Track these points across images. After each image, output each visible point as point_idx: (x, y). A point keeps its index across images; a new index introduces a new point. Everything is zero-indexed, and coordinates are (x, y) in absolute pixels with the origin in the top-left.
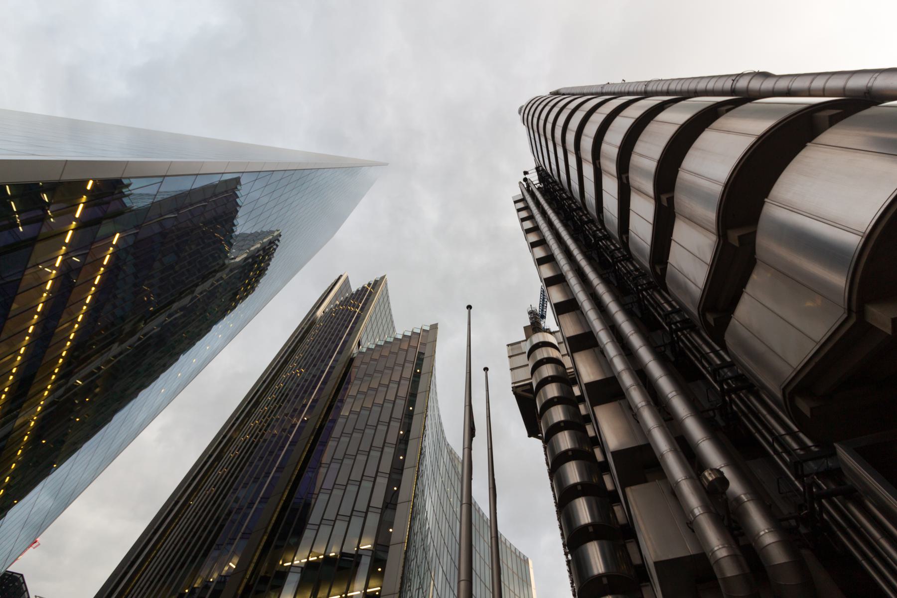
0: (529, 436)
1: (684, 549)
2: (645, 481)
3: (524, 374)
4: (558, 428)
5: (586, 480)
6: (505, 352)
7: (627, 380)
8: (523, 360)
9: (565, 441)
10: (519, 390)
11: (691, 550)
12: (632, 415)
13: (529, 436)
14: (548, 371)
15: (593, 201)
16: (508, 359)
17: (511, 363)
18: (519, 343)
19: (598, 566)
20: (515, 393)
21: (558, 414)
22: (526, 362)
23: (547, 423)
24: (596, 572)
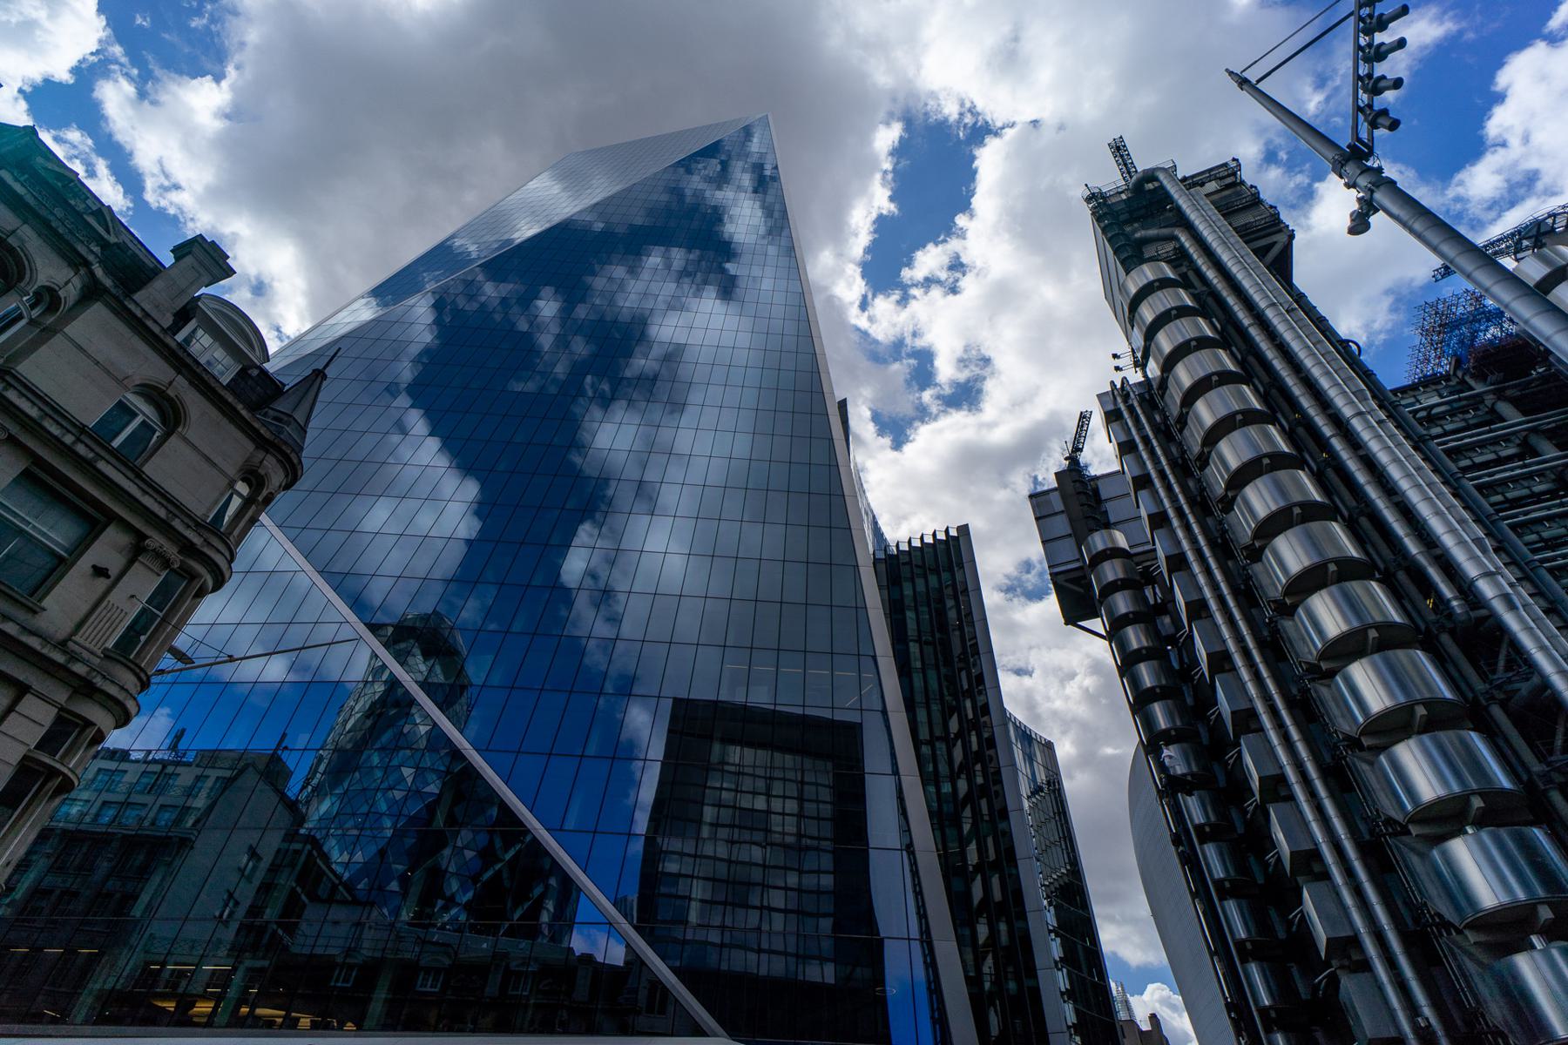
10: (1060, 579)
23: (1088, 551)
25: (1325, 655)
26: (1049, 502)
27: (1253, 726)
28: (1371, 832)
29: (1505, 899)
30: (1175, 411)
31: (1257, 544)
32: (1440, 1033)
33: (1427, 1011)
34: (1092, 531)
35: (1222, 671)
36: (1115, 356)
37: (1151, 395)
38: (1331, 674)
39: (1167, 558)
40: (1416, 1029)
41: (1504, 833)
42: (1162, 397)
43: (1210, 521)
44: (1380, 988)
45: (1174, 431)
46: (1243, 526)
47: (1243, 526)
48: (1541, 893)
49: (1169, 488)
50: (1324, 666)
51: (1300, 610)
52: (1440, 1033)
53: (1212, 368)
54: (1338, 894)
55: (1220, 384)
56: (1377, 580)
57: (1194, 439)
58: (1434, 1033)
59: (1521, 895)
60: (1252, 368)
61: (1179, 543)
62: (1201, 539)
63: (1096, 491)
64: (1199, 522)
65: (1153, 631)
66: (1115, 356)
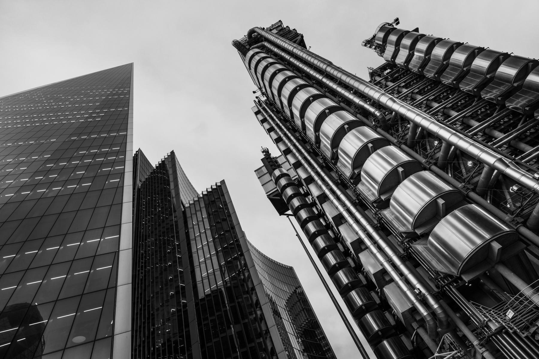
0: (262, 160)
1: (356, 238)
2: (326, 202)
3: (272, 186)
4: (299, 209)
5: (318, 229)
6: (255, 176)
7: (292, 148)
8: (267, 177)
9: (303, 214)
10: (271, 197)
11: (381, 268)
12: (306, 170)
13: (262, 160)
14: (283, 182)
15: (289, 115)
16: (258, 180)
17: (265, 189)
18: (261, 168)
19: (345, 280)
20: (270, 199)
21: (296, 202)
22: (269, 179)
23: (285, 197)
24: (333, 264)
25: (381, 192)
26: (262, 171)
27: (387, 279)
28: (438, 287)
29: (473, 247)
30: (328, 154)
31: (383, 198)
32: (426, 294)
33: (418, 286)
34: (274, 169)
35: (362, 250)
36: (254, 92)
37: (270, 103)
38: (425, 236)
39: (332, 218)
40: (416, 295)
41: (457, 212)
42: (319, 147)
43: (349, 192)
44: (375, 255)
45: (331, 165)
46: (369, 190)
47: (369, 190)
48: (487, 236)
49: (338, 199)
50: (419, 232)
51: (392, 201)
52: (426, 294)
53: (341, 122)
54: (399, 287)
55: (350, 129)
56: (394, 145)
57: (311, 133)
58: (424, 295)
59: (479, 242)
60: (312, 82)
61: (337, 208)
62: (295, 141)
63: (277, 162)
64: (292, 135)
65: (327, 238)
66: (254, 92)
